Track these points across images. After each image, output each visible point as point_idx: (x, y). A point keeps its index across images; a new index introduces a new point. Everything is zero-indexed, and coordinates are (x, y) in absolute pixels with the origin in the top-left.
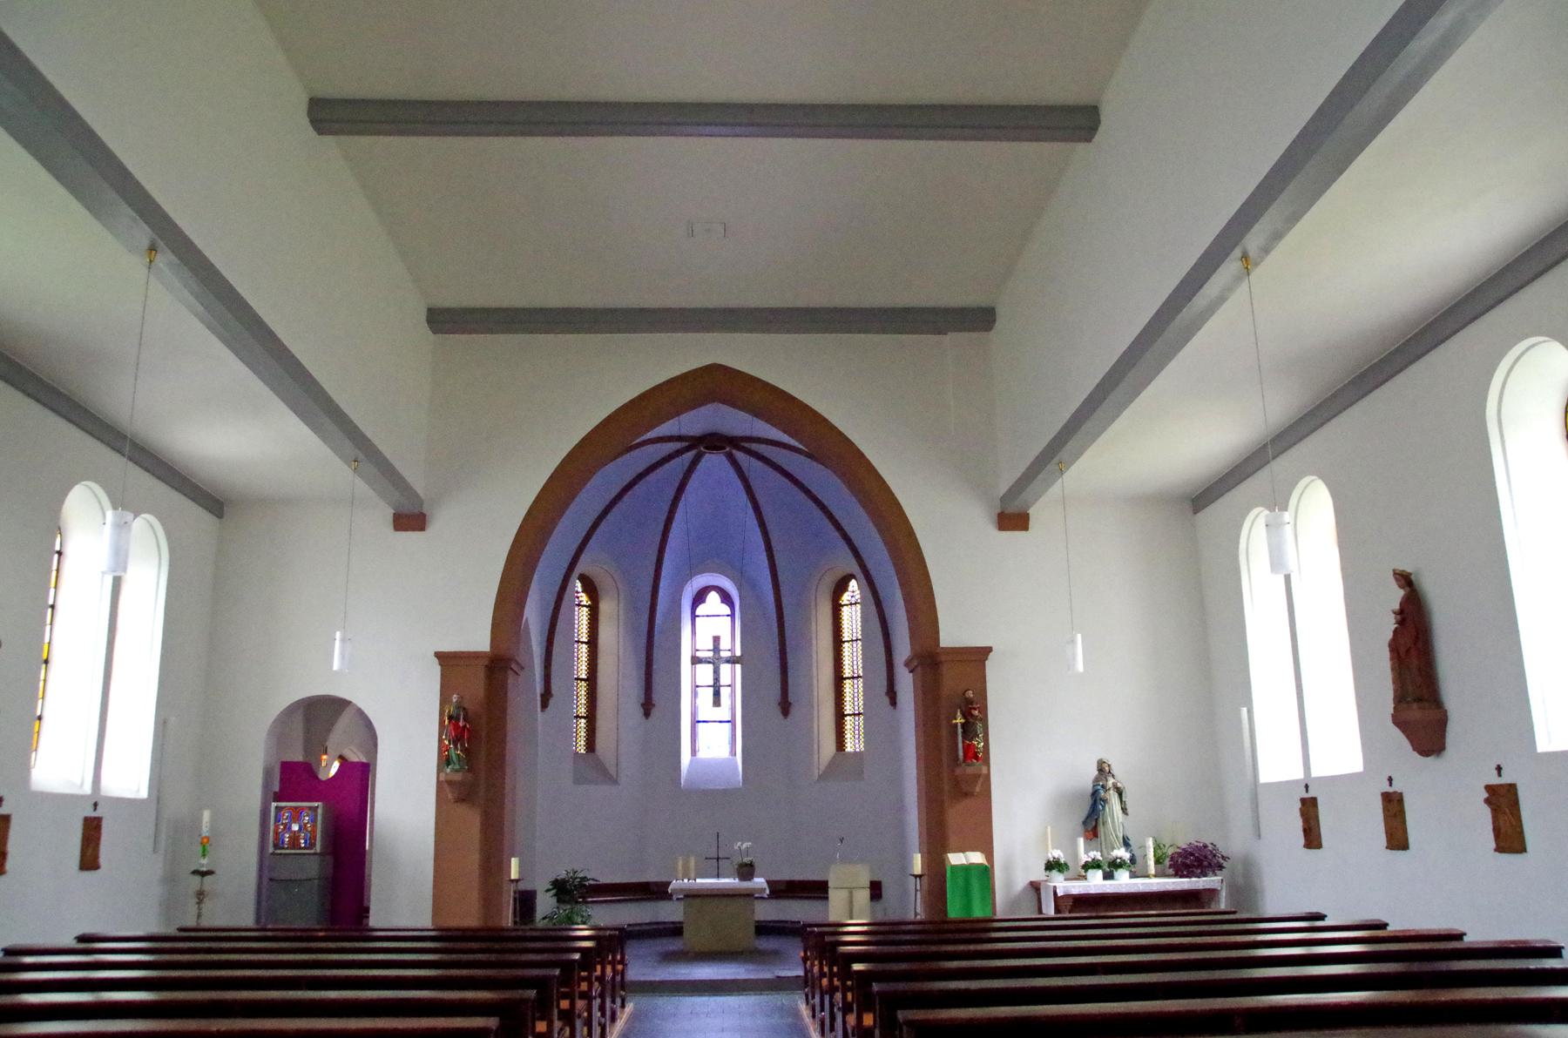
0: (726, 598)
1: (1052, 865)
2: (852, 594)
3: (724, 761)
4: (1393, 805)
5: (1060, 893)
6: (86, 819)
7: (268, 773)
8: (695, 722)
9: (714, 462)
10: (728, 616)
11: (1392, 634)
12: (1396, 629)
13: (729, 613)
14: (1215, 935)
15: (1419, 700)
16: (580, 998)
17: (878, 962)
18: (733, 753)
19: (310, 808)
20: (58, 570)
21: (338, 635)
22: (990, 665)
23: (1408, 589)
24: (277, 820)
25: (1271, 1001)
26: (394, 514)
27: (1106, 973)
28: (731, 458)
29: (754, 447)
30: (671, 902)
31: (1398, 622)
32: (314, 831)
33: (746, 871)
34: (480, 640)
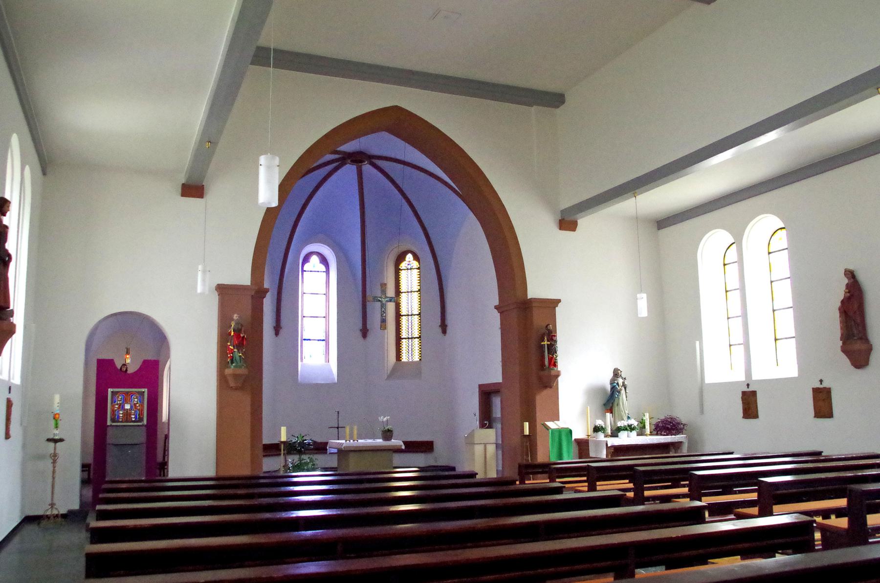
0: (324, 261)
1: (597, 429)
2: (408, 263)
5: (609, 445)
10: (324, 272)
14: (674, 464)
17: (422, 490)
19: (138, 393)
21: (200, 267)
22: (559, 310)
23: (852, 280)
24: (113, 401)
25: (333, 511)
27: (189, 500)
29: (379, 163)
30: (326, 455)
32: (142, 411)
33: (387, 434)
34: (242, 276)
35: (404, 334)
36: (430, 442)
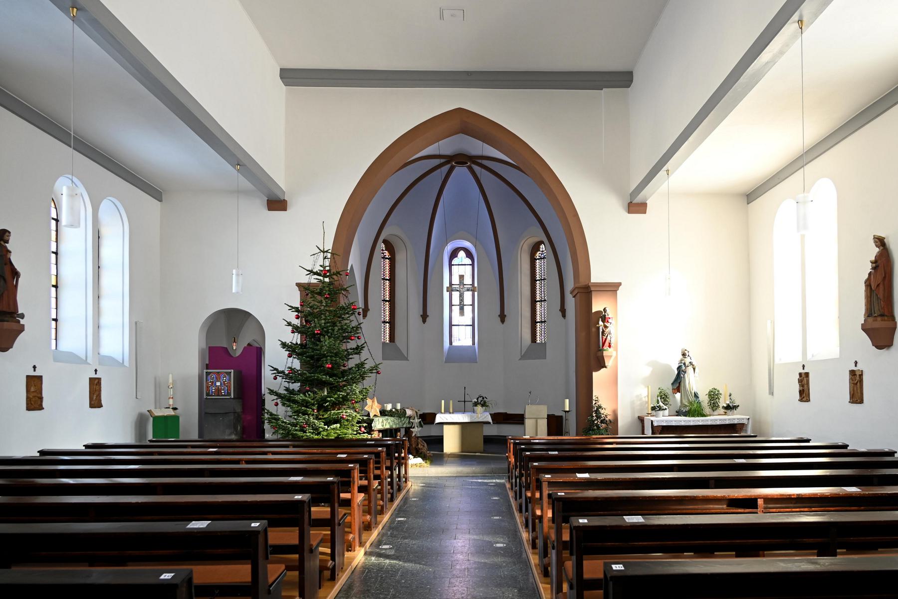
0: (469, 255)
3: (469, 347)
4: (856, 379)
6: (91, 379)
7: (201, 353)
8: (451, 325)
9: (461, 172)
11: (868, 275)
12: (871, 272)
13: (471, 263)
15: (882, 315)
16: (360, 491)
18: (474, 343)
19: (226, 373)
20: (57, 231)
23: (882, 248)
26: (267, 200)
28: (470, 169)
29: (485, 162)
31: (873, 268)
35: (538, 319)
36: (560, 416)
